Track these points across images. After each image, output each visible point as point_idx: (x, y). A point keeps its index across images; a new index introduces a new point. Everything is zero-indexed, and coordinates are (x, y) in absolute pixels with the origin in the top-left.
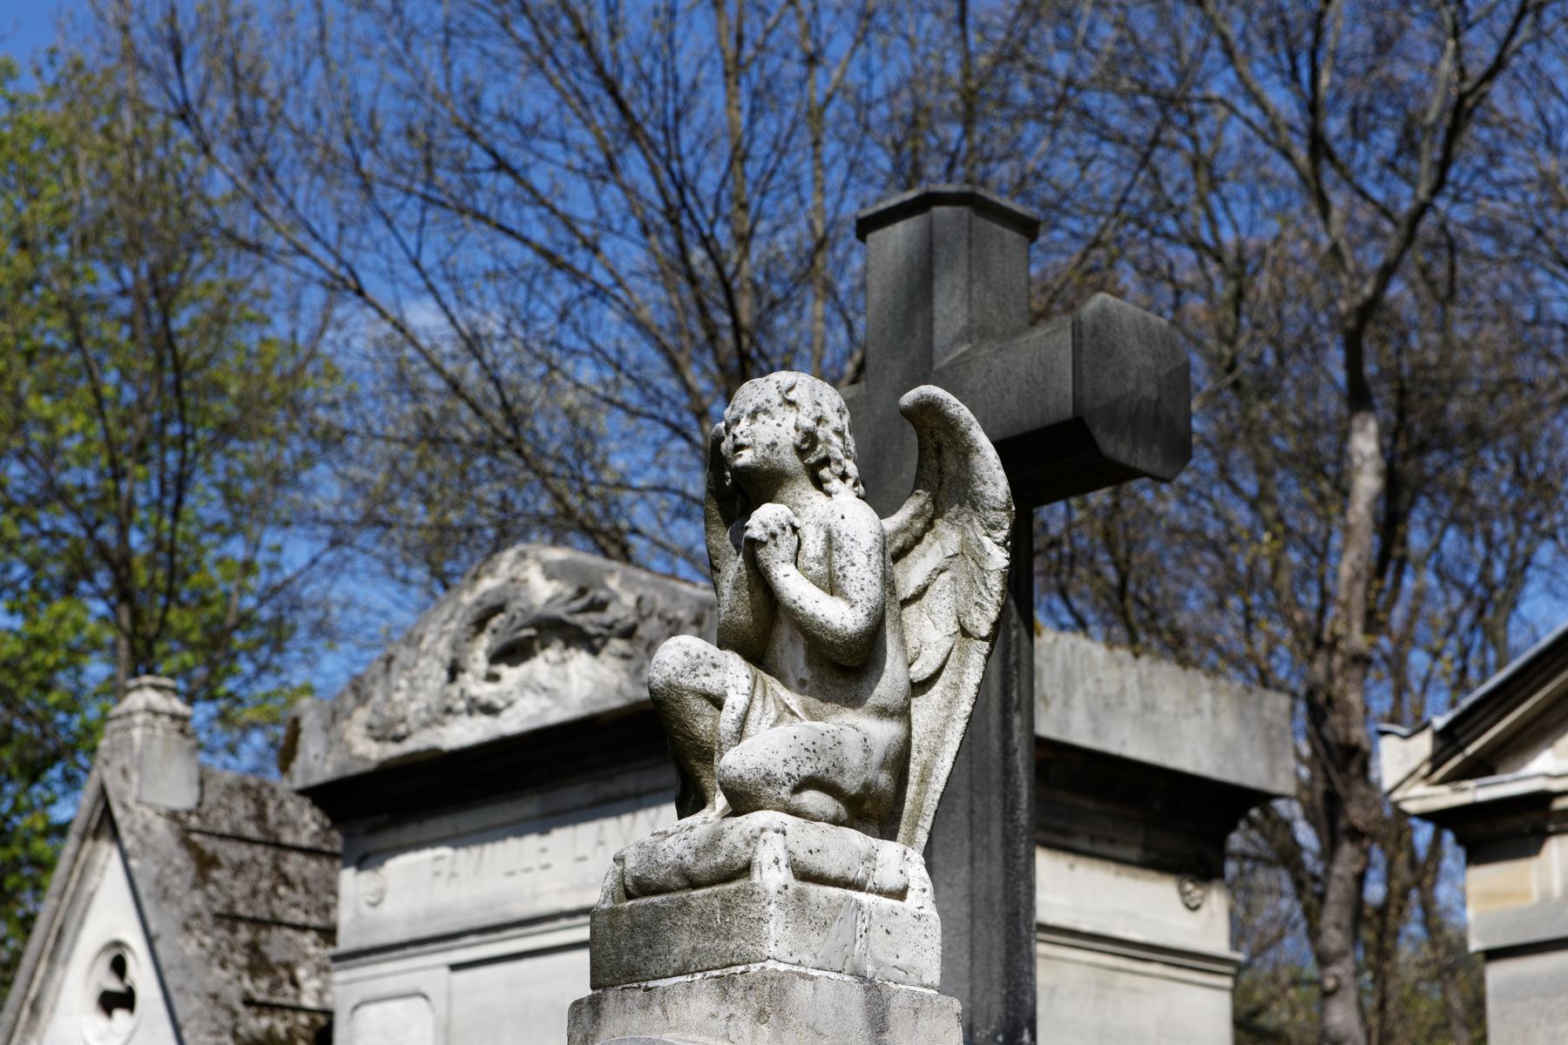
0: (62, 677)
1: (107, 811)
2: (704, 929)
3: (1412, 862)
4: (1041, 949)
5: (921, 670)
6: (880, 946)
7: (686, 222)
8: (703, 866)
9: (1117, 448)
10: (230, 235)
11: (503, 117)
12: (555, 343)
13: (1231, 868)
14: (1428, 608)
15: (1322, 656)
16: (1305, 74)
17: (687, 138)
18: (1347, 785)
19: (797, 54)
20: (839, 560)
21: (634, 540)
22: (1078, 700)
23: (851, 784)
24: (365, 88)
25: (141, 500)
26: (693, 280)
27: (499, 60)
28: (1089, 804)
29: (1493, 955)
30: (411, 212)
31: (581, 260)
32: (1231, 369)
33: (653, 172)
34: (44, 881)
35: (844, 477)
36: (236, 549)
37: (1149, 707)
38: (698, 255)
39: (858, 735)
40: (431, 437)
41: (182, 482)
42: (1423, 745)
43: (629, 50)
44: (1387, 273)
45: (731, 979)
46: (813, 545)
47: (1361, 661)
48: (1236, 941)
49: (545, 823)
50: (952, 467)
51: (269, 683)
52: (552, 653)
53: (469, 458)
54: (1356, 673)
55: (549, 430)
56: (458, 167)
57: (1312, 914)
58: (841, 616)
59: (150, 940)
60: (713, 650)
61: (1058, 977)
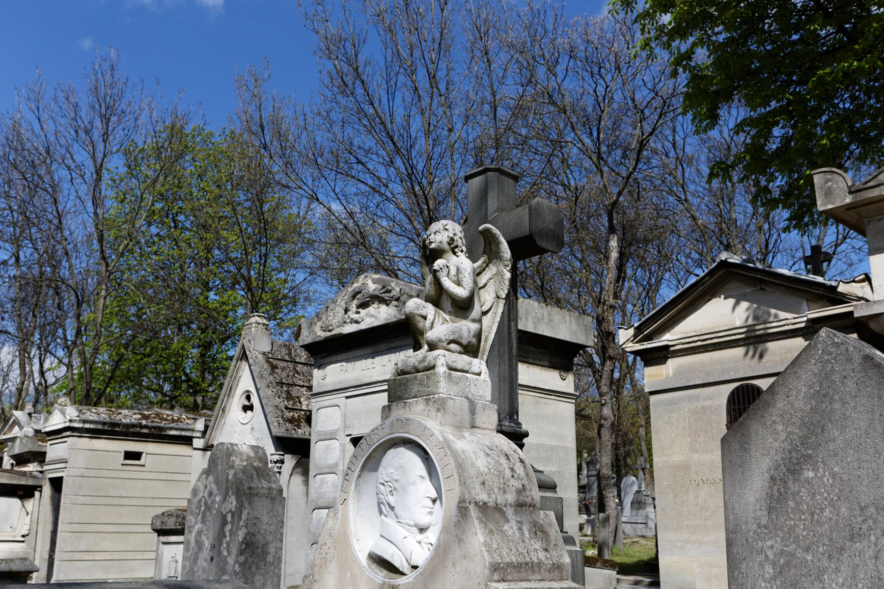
0: (231, 313)
1: (245, 351)
2: (421, 384)
3: (628, 366)
4: (520, 391)
5: (485, 308)
6: (473, 389)
7: (413, 178)
8: (421, 366)
9: (542, 243)
10: (279, 183)
11: (359, 147)
12: (375, 214)
13: (575, 368)
14: (632, 292)
15: (601, 306)
16: (595, 134)
17: (414, 154)
18: (608, 344)
19: (446, 128)
20: (461, 276)
21: (399, 272)
22: (530, 318)
23: (465, 342)
24: (318, 139)
25: (254, 261)
26: (416, 196)
27: (358, 130)
28: (533, 349)
29: (652, 393)
30: (333, 175)
31: (383, 189)
32: (574, 222)
33: (404, 163)
34: (464, 538)
35: (462, 251)
36: (282, 275)
37: (551, 320)
38: (417, 188)
39: (466, 328)
40: (338, 242)
41: (266, 256)
42: (631, 331)
43: (396, 129)
44: (620, 194)
45: (429, 399)
46: (453, 271)
47: (613, 307)
48: (576, 389)
49: (373, 355)
50: (494, 248)
51: (292, 315)
52: (375, 305)
53: (350, 248)
54: (611, 311)
55: (373, 240)
56: (346, 162)
57: (598, 381)
58: (462, 292)
59: (257, 390)
60: (423, 302)
61: (525, 400)
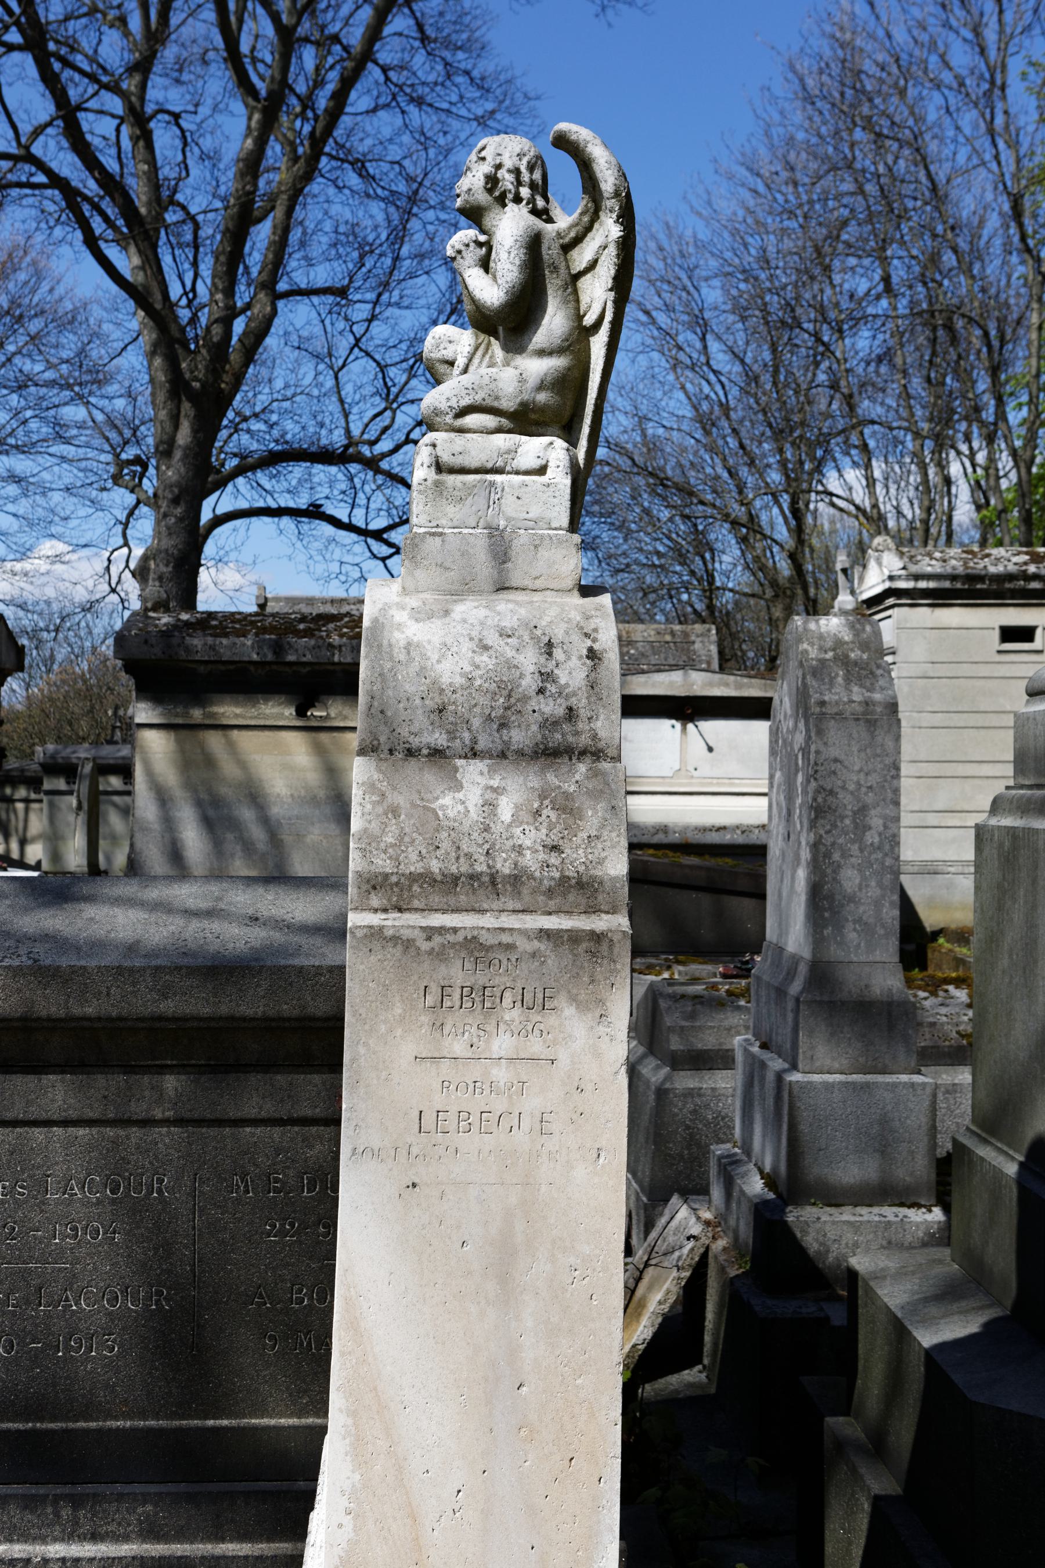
23: (508, 404)
